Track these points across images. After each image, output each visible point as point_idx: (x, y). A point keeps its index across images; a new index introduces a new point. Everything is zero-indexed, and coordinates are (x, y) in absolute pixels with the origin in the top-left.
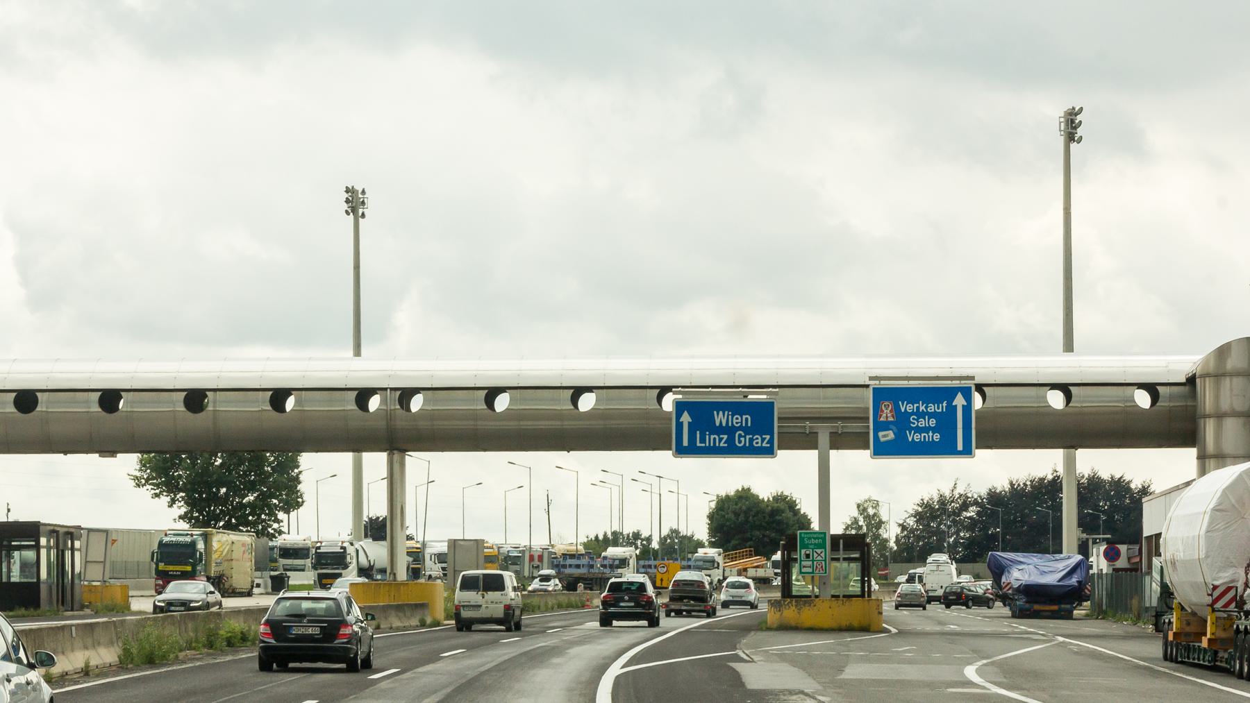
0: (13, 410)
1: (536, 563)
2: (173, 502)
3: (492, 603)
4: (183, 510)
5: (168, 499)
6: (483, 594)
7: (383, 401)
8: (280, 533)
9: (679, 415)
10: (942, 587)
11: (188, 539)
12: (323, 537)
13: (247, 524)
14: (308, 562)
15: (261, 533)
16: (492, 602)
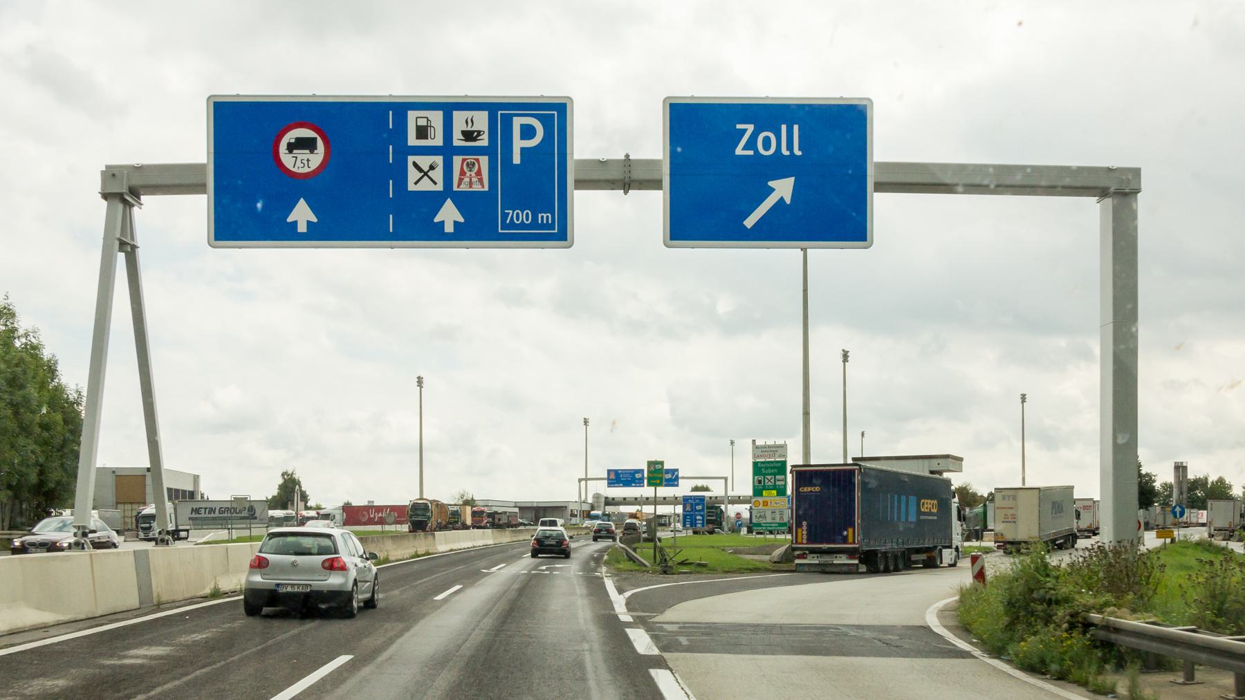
12: (430, 495)
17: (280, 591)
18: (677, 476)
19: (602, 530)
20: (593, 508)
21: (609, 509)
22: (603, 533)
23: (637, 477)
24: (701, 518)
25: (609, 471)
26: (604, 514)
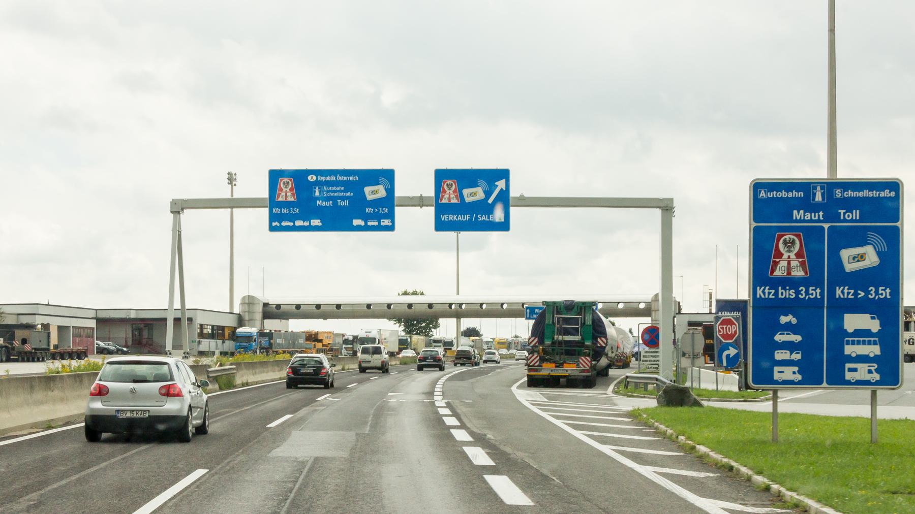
0: (315, 308)
1: (516, 345)
2: (400, 326)
3: (376, 360)
4: (403, 329)
5: (399, 325)
7: (455, 306)
8: (433, 335)
9: (526, 310)
11: (405, 338)
13: (422, 333)
14: (441, 344)
15: (427, 335)
17: (121, 417)
18: (504, 197)
19: (427, 358)
20: (241, 321)
21: (271, 325)
22: (429, 361)
23: (370, 197)
24: (874, 325)
25: (275, 176)
26: (262, 334)
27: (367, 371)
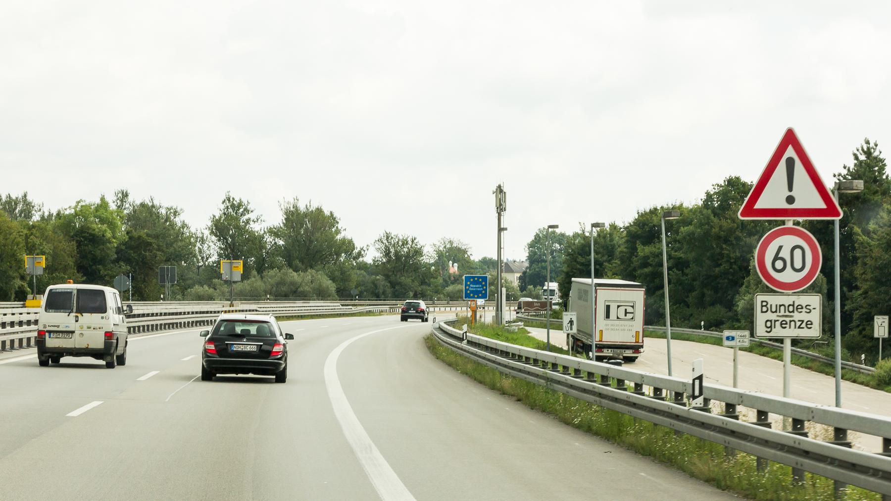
6: (77, 317)
10: (696, 404)
16: (89, 328)
27: (64, 360)
